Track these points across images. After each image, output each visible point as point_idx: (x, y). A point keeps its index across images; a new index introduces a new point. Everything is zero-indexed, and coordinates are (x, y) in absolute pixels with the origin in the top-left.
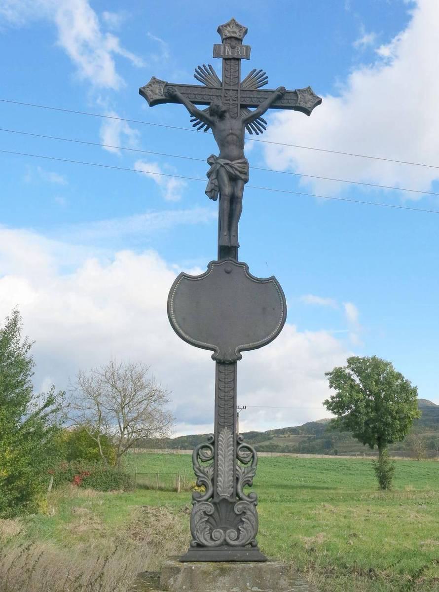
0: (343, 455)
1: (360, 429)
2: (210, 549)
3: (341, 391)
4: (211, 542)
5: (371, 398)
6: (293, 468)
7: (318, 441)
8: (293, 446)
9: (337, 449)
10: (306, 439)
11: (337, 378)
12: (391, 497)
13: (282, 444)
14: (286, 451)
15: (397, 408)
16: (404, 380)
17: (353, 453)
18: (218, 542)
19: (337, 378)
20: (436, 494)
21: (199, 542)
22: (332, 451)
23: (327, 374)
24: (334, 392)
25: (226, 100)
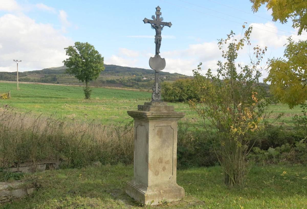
0: (61, 84)
1: (79, 73)
3: (71, 57)
5: (84, 60)
6: (43, 89)
7: (49, 77)
8: (38, 79)
9: (58, 81)
10: (44, 76)
11: (70, 50)
12: (91, 102)
13: (32, 78)
14: (34, 81)
15: (95, 66)
16: (99, 54)
17: (66, 83)
19: (70, 50)
20: (108, 101)
22: (56, 82)
23: (65, 49)
24: (68, 57)
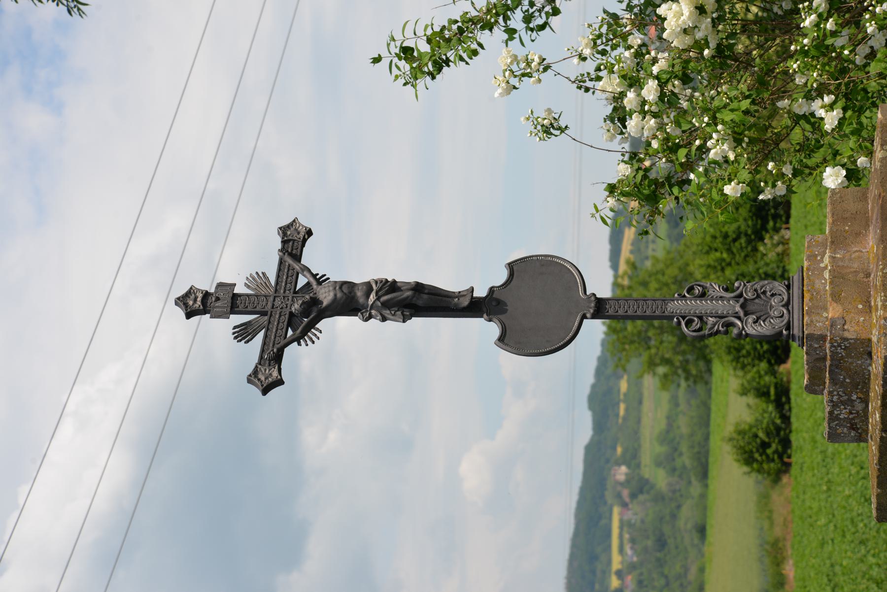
2: (791, 319)
4: (784, 317)
18: (785, 311)
21: (785, 327)
25: (287, 307)
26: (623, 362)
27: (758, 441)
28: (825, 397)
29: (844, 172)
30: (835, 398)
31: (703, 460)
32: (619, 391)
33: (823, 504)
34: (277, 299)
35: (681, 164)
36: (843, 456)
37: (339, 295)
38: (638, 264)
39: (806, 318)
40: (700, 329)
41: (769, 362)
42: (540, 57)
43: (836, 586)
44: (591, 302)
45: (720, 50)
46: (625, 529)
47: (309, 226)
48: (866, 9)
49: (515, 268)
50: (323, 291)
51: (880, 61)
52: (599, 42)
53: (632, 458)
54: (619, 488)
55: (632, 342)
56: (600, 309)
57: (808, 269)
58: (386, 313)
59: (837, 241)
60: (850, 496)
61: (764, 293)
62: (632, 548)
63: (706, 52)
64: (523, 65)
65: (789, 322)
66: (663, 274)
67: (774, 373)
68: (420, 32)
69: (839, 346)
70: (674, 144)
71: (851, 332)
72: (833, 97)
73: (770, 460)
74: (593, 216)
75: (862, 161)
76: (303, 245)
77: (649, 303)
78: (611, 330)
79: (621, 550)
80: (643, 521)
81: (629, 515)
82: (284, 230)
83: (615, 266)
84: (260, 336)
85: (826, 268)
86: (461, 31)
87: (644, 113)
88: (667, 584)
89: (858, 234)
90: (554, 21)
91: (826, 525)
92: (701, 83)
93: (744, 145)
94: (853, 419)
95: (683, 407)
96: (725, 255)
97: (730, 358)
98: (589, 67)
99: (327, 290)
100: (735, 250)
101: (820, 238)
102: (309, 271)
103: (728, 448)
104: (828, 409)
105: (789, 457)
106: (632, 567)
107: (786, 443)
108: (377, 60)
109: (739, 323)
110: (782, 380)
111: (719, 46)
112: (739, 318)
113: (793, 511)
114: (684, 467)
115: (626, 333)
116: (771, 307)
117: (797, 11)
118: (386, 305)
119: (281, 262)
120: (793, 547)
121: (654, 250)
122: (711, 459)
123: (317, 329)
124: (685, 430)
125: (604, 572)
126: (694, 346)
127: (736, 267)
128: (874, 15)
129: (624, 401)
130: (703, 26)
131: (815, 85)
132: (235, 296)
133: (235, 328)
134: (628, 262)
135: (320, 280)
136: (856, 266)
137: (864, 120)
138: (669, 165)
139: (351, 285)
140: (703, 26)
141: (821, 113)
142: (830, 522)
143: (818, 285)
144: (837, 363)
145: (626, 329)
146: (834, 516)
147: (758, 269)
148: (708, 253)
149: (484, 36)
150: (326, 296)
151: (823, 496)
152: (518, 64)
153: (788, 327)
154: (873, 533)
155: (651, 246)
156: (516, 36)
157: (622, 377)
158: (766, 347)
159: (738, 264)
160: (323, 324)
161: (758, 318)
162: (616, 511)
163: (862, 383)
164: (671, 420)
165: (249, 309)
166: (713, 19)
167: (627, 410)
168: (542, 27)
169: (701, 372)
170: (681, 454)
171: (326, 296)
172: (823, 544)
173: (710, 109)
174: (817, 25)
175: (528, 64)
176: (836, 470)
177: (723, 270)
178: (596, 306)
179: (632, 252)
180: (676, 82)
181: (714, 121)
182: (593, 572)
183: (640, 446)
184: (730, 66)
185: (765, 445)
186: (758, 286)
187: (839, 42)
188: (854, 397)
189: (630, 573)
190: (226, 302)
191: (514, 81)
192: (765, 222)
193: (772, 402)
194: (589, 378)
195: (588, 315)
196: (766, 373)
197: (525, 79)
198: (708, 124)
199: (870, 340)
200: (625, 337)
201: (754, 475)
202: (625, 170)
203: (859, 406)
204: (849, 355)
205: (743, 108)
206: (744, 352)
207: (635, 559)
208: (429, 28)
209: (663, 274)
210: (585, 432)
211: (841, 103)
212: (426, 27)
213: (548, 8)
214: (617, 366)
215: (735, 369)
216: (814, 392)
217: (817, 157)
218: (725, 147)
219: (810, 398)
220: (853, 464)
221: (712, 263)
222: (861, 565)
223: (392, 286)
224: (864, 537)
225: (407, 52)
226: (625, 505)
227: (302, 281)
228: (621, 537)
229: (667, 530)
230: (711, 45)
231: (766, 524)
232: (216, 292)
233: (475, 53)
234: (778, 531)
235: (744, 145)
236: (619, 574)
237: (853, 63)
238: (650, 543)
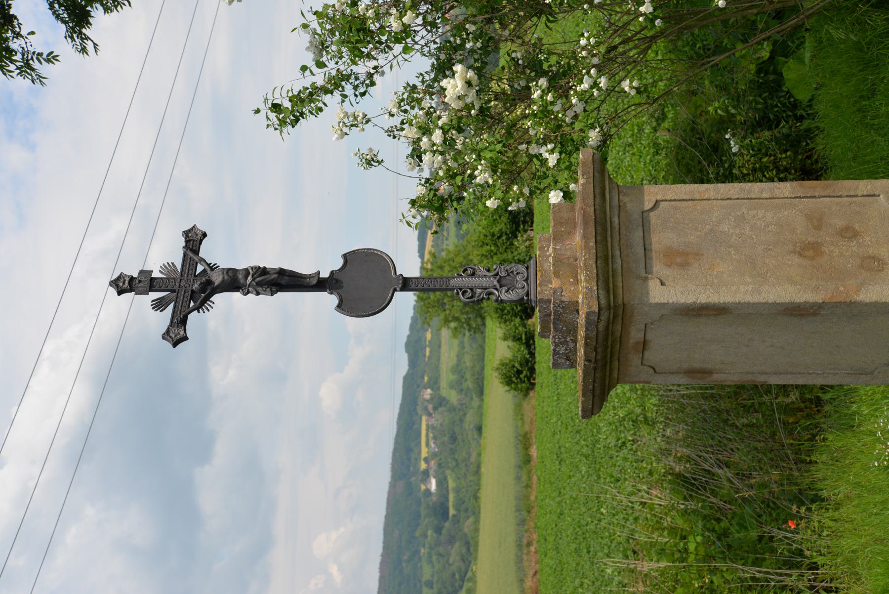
26: (428, 320)
27: (515, 369)
28: (551, 340)
29: (562, 194)
30: (557, 340)
31: (481, 383)
32: (426, 339)
33: (554, 409)
34: (183, 281)
35: (459, 187)
36: (567, 377)
37: (226, 278)
38: (437, 255)
39: (538, 288)
40: (471, 297)
41: (521, 318)
42: (363, 114)
43: (561, 460)
44: (399, 280)
45: (482, 110)
46: (430, 430)
47: (204, 230)
48: (571, 88)
49: (348, 258)
50: (215, 275)
51: (580, 121)
52: (402, 104)
53: (434, 384)
54: (426, 404)
55: (433, 307)
56: (406, 284)
57: (539, 256)
58: (260, 289)
59: (557, 238)
60: (570, 403)
61: (512, 272)
62: (434, 443)
63: (473, 112)
64: (351, 119)
65: (528, 291)
66: (453, 261)
67: (525, 326)
68: (284, 95)
69: (559, 306)
70: (454, 173)
71: (566, 297)
72: (553, 145)
73: (523, 382)
74: (401, 221)
75: (572, 186)
76: (200, 244)
77: (438, 280)
78: (420, 299)
79: (427, 444)
80: (441, 425)
81: (432, 421)
82: (186, 233)
83: (422, 256)
84: (171, 306)
85: (550, 255)
86: (311, 94)
87: (434, 152)
88: (457, 465)
89: (570, 233)
90: (371, 89)
91: (556, 422)
92: (470, 133)
93: (498, 174)
94: (568, 353)
95: (467, 349)
96: (493, 248)
97: (497, 316)
98: (396, 121)
99: (217, 274)
100: (499, 245)
101: (546, 235)
102: (205, 261)
103: (496, 374)
104: (552, 348)
105: (534, 379)
106: (435, 455)
107: (532, 370)
108: (257, 111)
109: (496, 292)
110: (529, 330)
111: (481, 107)
112: (496, 289)
113: (536, 414)
114: (468, 388)
115: (429, 301)
116: (517, 281)
117: (529, 88)
118: (259, 284)
119: (185, 255)
120: (536, 437)
121: (447, 245)
122: (485, 383)
123: (211, 302)
124: (468, 364)
125: (416, 459)
126: (474, 308)
127: (499, 255)
128: (576, 91)
129: (429, 346)
130: (471, 95)
131: (542, 136)
132: (152, 280)
133: (153, 301)
134: (430, 253)
135: (212, 268)
136: (568, 253)
137: (572, 160)
138: (451, 187)
139: (235, 271)
140: (471, 95)
141: (546, 155)
142: (559, 420)
143: (546, 266)
144: (558, 317)
145: (429, 298)
146: (561, 415)
147: (514, 257)
148: (482, 246)
149: (327, 98)
150: (217, 279)
151: (555, 404)
152: (348, 118)
153: (527, 295)
154: (584, 425)
155: (445, 242)
156: (347, 100)
157: (428, 330)
158: (519, 308)
159: (501, 253)
160: (216, 298)
161: (509, 289)
162: (424, 418)
163: (573, 330)
164: (460, 357)
165: (163, 288)
166: (477, 91)
167: (431, 352)
168: (363, 94)
169: (478, 325)
170: (466, 380)
171: (217, 279)
172: (554, 434)
173: (476, 150)
174: (542, 97)
175: (355, 118)
176: (562, 387)
177: (492, 257)
178: (403, 283)
179: (433, 246)
180: (454, 132)
181: (479, 158)
182: (409, 460)
183: (439, 375)
184: (488, 122)
185: (519, 372)
186: (508, 268)
187: (556, 108)
188: (568, 339)
189: (433, 459)
190: (145, 284)
191: (345, 130)
192: (518, 226)
193: (523, 344)
194: (406, 332)
195: (398, 289)
196: (519, 326)
197: (353, 128)
198: (475, 160)
199: (577, 302)
200: (429, 303)
201: (512, 392)
202: (422, 190)
203: (571, 345)
204: (565, 312)
205: (498, 150)
206: (506, 311)
207: (436, 450)
208: (290, 92)
209: (453, 261)
210: (403, 367)
211: (558, 149)
212: (288, 91)
213: (368, 82)
214: (424, 323)
215: (500, 323)
216: (544, 337)
217: (546, 182)
218: (487, 175)
219: (546, 341)
220: (572, 382)
221: (485, 253)
222: (577, 446)
223: (264, 271)
224: (579, 428)
225: (276, 107)
226: (430, 415)
227: (200, 268)
228: (427, 436)
229: (457, 429)
230: (476, 107)
231: (520, 423)
232: (139, 277)
233: (321, 110)
234: (527, 428)
235: (498, 174)
236: (426, 460)
237: (565, 122)
238: (446, 439)
